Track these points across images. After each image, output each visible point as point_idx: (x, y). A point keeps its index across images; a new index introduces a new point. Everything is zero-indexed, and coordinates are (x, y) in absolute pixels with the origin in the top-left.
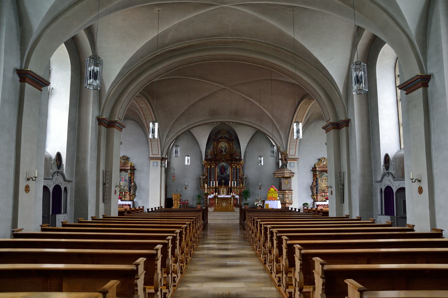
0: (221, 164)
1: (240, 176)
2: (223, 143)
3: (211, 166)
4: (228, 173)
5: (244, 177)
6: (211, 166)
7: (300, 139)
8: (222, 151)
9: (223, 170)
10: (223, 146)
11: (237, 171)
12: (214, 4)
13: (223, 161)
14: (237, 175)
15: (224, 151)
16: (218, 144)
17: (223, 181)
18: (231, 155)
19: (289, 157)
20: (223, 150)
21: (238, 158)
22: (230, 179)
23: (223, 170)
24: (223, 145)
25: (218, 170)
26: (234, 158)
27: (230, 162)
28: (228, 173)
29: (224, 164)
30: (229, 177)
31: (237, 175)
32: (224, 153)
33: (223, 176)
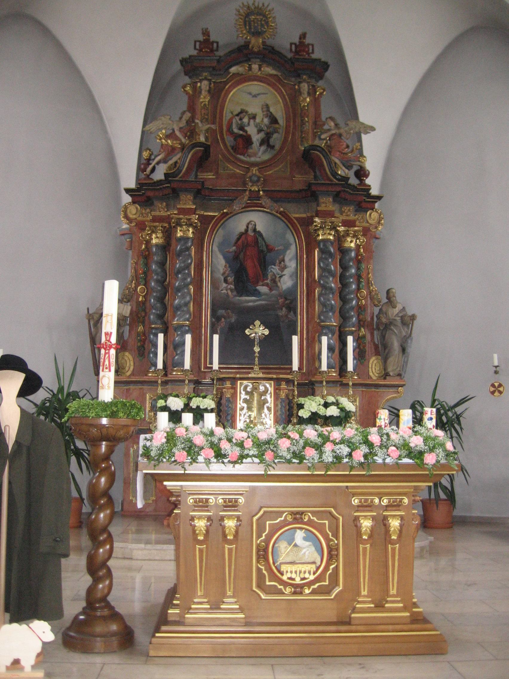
0: (239, 224)
1: (360, 309)
2: (255, 87)
3: (168, 234)
4: (286, 283)
5: (393, 312)
6: (168, 234)
7: (296, 334)
8: (247, 141)
9: (251, 261)
10: (254, 108)
11: (345, 268)
12: (71, 476)
13: (254, 203)
14: (344, 300)
15: (256, 138)
16: (218, 93)
17: (259, 331)
18: (309, 159)
19: (114, 434)
20: (252, 130)
21: (221, 312)
22: (302, 319)
23: (251, 261)
24: (253, 100)
25: (221, 263)
26: (322, 179)
27: (297, 213)
28: (286, 283)
29: (260, 221)
30: (292, 308)
31: (344, 300)
32: (259, 154)
33: (249, 301)
